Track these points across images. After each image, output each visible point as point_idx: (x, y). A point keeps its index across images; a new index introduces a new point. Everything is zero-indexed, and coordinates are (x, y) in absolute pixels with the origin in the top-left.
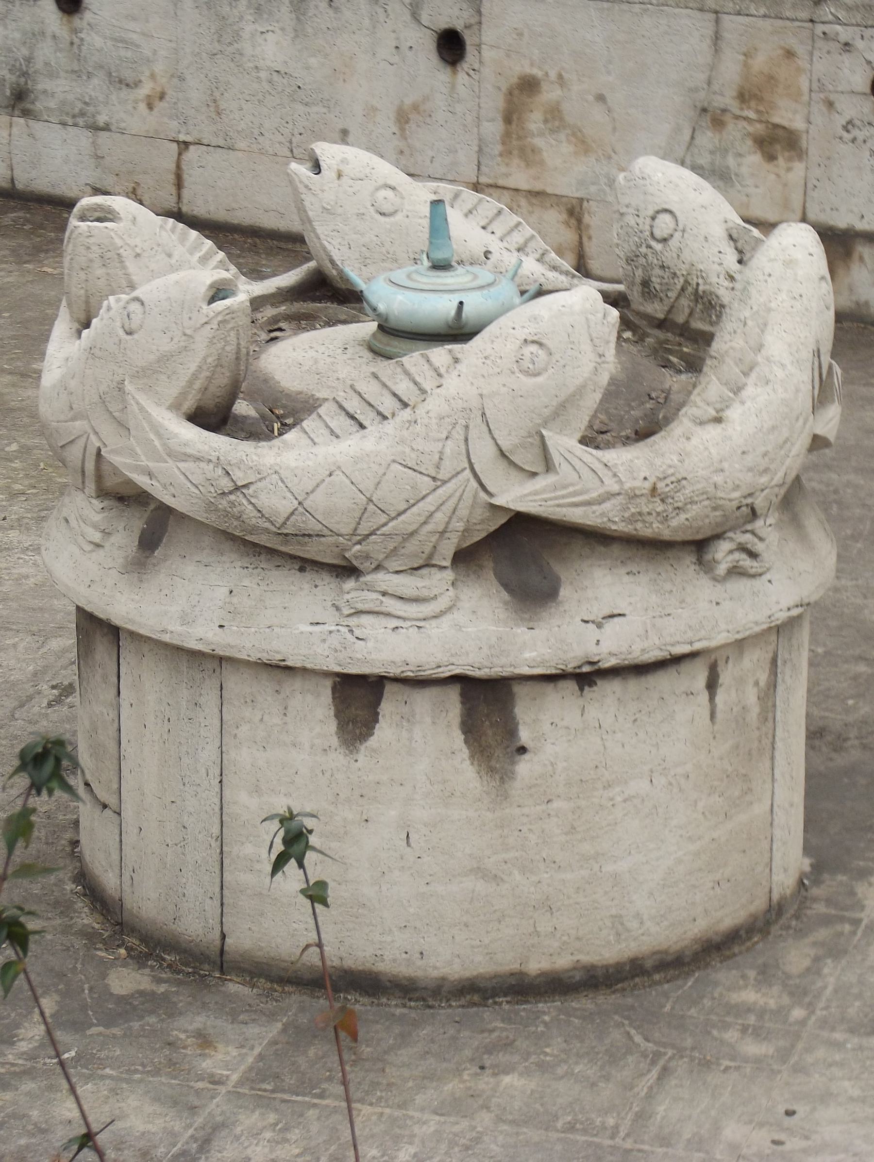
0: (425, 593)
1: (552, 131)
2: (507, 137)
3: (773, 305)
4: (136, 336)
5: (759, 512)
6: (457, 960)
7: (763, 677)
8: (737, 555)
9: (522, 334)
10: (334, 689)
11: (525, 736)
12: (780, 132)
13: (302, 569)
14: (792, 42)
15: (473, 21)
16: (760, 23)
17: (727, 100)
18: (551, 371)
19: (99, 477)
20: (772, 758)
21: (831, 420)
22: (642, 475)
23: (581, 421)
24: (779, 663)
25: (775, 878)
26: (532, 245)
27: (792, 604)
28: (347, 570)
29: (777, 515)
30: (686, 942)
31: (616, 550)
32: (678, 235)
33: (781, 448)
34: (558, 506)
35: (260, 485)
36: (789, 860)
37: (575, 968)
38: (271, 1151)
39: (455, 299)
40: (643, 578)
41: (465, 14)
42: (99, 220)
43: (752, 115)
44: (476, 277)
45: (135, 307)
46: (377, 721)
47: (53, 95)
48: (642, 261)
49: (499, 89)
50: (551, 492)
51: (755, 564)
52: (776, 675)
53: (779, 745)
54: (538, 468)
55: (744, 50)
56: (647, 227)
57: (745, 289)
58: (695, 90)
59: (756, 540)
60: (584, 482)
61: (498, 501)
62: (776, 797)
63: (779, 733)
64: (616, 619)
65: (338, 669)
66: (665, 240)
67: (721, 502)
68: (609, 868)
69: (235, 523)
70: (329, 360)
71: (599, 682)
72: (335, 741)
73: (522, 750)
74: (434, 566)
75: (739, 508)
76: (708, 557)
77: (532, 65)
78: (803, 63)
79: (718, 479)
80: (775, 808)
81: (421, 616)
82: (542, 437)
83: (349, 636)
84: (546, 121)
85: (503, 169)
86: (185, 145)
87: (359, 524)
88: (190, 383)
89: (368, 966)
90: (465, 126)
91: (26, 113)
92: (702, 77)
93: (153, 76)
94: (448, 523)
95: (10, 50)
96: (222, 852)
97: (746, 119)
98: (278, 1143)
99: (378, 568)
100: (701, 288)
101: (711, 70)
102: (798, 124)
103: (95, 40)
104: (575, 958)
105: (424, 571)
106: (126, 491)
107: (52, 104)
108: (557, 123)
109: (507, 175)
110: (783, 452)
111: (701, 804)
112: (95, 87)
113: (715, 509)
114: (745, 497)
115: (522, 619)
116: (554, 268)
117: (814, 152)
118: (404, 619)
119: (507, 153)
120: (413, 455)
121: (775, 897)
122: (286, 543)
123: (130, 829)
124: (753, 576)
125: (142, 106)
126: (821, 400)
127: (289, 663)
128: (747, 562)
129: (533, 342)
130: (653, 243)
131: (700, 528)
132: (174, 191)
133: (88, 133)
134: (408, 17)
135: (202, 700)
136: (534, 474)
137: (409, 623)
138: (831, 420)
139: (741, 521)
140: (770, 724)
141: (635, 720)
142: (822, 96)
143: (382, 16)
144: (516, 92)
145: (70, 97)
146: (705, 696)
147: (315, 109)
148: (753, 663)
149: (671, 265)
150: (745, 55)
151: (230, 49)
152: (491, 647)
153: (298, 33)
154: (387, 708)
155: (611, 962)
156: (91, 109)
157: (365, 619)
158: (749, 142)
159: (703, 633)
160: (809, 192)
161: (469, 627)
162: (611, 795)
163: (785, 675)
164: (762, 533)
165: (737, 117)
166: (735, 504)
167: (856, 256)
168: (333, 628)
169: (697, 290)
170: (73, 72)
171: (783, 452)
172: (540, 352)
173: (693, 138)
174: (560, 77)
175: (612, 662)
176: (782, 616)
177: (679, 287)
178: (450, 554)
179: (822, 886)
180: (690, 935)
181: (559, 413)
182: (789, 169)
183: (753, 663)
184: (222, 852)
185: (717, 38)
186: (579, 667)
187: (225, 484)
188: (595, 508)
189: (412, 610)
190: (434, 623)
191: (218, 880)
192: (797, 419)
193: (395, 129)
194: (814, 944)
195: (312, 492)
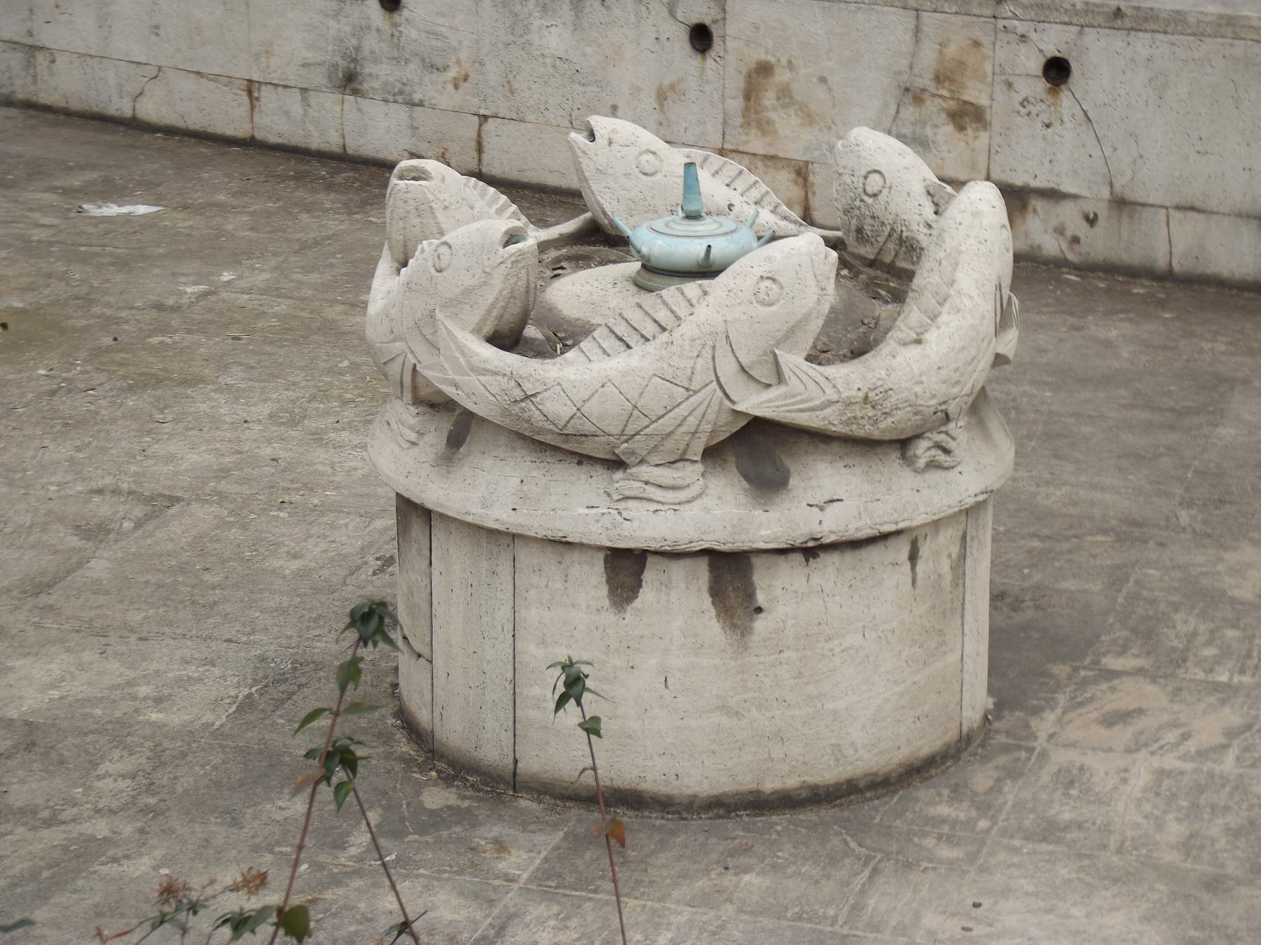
0: (680, 482)
1: (783, 107)
2: (747, 110)
4: (444, 273)
7: (955, 551)
9: (759, 272)
11: (761, 598)
12: (969, 108)
13: (580, 463)
14: (978, 34)
15: (719, 17)
16: (953, 18)
17: (926, 81)
18: (782, 302)
19: (415, 388)
20: (963, 617)
25: (964, 714)
26: (767, 199)
27: (978, 491)
28: (616, 464)
31: (835, 447)
32: (885, 191)
36: (976, 700)
38: (555, 936)
41: (713, 12)
43: (946, 93)
45: (444, 249)
46: (641, 586)
53: (968, 606)
58: (900, 73)
60: (810, 392)
61: (739, 408)
65: (609, 544)
72: (606, 603)
73: (759, 610)
76: (910, 453)
78: (987, 51)
81: (676, 501)
82: (775, 355)
83: (618, 517)
84: (778, 99)
85: (744, 138)
88: (489, 311)
89: (634, 786)
91: (355, 92)
93: (458, 62)
94: (698, 425)
97: (941, 96)
99: (642, 462)
102: (983, 101)
103: (411, 33)
105: (680, 465)
107: (377, 85)
108: (787, 100)
109: (747, 142)
111: (904, 654)
112: (412, 71)
113: (915, 414)
116: (785, 218)
117: (996, 124)
118: (663, 503)
119: (746, 125)
121: (965, 729)
122: (567, 441)
124: (947, 469)
125: (450, 87)
127: (569, 539)
128: (941, 457)
129: (768, 278)
130: (866, 198)
132: (475, 155)
134: (665, 14)
135: (499, 569)
136: (769, 386)
137: (667, 507)
140: (961, 589)
143: (645, 14)
144: (754, 75)
145: (391, 79)
146: (907, 566)
147: (590, 89)
148: (947, 540)
151: (521, 40)
153: (577, 27)
154: (648, 576)
156: (408, 89)
157: (631, 504)
158: (944, 116)
159: (906, 515)
160: (993, 156)
161: (717, 511)
163: (973, 549)
165: (934, 95)
166: (932, 410)
167: (1030, 208)
170: (394, 58)
173: (897, 112)
174: (790, 62)
180: (895, 760)
181: (789, 336)
182: (976, 138)
183: (947, 540)
187: (518, 394)
190: (687, 506)
193: (655, 105)
194: (997, 768)
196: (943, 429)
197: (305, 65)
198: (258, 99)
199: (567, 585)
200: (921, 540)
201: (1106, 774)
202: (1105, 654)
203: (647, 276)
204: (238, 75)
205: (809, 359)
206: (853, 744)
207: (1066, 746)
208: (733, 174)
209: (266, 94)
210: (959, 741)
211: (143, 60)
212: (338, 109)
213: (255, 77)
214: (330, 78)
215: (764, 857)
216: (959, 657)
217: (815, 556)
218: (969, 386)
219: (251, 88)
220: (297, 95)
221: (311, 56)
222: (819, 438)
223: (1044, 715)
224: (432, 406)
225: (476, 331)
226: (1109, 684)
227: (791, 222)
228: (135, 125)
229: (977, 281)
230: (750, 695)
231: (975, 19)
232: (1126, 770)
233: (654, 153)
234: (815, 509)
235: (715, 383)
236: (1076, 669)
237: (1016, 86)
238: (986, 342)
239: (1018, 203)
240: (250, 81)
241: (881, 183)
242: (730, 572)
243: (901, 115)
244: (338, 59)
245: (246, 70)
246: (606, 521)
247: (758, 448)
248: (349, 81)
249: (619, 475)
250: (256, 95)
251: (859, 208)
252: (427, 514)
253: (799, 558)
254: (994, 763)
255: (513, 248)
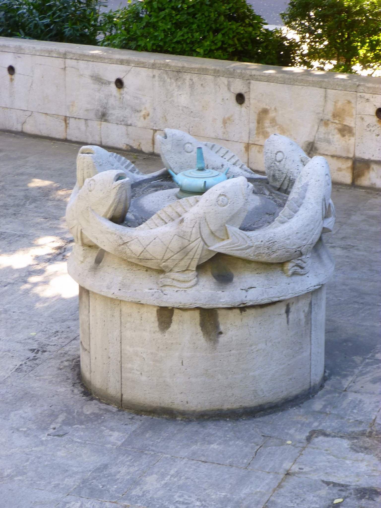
0: (187, 279)
1: (273, 126)
2: (258, 128)
3: (309, 183)
4: (92, 192)
5: (303, 253)
6: (199, 405)
7: (307, 309)
8: (296, 268)
9: (219, 192)
10: (157, 311)
11: (222, 328)
12: (347, 128)
13: (147, 271)
14: (349, 98)
15: (247, 91)
16: (339, 92)
17: (329, 116)
18: (229, 205)
19: (82, 239)
20: (310, 337)
21: (330, 222)
22: (261, 240)
23: (240, 221)
24: (313, 304)
25: (312, 378)
26: (238, 163)
27: (316, 284)
28: (161, 271)
29: (310, 254)
30: (279, 400)
31: (253, 265)
32: (284, 160)
33: (311, 231)
34: (232, 250)
35: (132, 242)
36: (317, 371)
37: (240, 408)
38: (128, 469)
39: (204, 180)
40: (263, 275)
41: (245, 89)
42: (88, 153)
43: (337, 122)
44: (212, 173)
45: (92, 182)
46: (171, 322)
47: (114, 115)
48: (272, 168)
49: (256, 112)
50: (229, 245)
51: (303, 271)
52: (311, 308)
53: (313, 332)
54: (226, 238)
55: (334, 101)
56: (274, 157)
57: (300, 178)
58: (318, 113)
59: (302, 263)
60: (234, 243)
61: (211, 248)
62: (312, 350)
63: (313, 328)
64: (253, 289)
65: (158, 305)
66: (280, 161)
67: (289, 250)
68: (251, 374)
69: (124, 255)
70: (163, 200)
71: (247, 310)
72: (157, 329)
73: (221, 333)
74: (190, 270)
75: (296, 252)
76: (285, 268)
77: (266, 105)
78: (353, 105)
79: (288, 242)
80: (312, 354)
81: (186, 287)
82: (226, 227)
83: (161, 293)
84: (271, 123)
85: (257, 139)
86: (155, 131)
87: (164, 255)
88: (109, 208)
89: (169, 406)
90: (245, 125)
91: (106, 121)
92: (322, 109)
93: (145, 108)
94: (194, 256)
95: (101, 101)
96: (121, 367)
97: (335, 123)
98: (131, 466)
99: (171, 271)
100: (291, 177)
101: (324, 107)
102: (352, 125)
103: (127, 97)
104: (241, 404)
105: (187, 272)
106: (91, 244)
107: (114, 117)
108: (274, 124)
109: (258, 141)
110: (311, 233)
111: (284, 352)
112: (127, 112)
113: (287, 252)
114: (298, 248)
115: (220, 288)
116: (246, 170)
117: (357, 134)
118: (180, 288)
119: (258, 134)
120: (182, 233)
121: (312, 384)
122: (141, 262)
123: (93, 358)
124: (302, 275)
125: (142, 118)
126: (326, 216)
127: (142, 302)
128: (299, 270)
129: (223, 195)
130: (276, 162)
131: (282, 258)
132: (152, 145)
133: (125, 127)
134: (226, 89)
135: (115, 314)
136: (223, 240)
137: (182, 289)
138: (330, 222)
139: (297, 256)
140: (309, 325)
141: (260, 324)
142: (360, 116)
143: (218, 89)
144: (261, 114)
145: (119, 115)
146: (285, 316)
147: (196, 119)
148: (303, 305)
149: (282, 170)
150: (335, 102)
151: (170, 100)
152: (209, 298)
153: (191, 95)
154: (174, 318)
155: (252, 406)
156: (126, 119)
157: (167, 288)
158: (336, 131)
159: (283, 294)
160: (356, 147)
161: (206, 292)
162: (252, 348)
163: (315, 309)
164: (305, 260)
165: (333, 122)
166: (294, 250)
167: (371, 169)
168: (157, 291)
169: (290, 178)
170: (120, 107)
171: (311, 233)
172: (225, 198)
173: (318, 129)
174: (275, 109)
175: (251, 303)
176: (313, 288)
177: (284, 177)
178: (195, 266)
179: (331, 381)
180: (281, 397)
181: (231, 219)
182: (349, 140)
183: (303, 305)
184: (121, 367)
185: (326, 97)
186: (239, 305)
187: (120, 242)
188: (244, 251)
189: (183, 285)
190: (190, 289)
191: (120, 376)
192: (317, 222)
193: (222, 125)
194: (325, 400)
195: (149, 244)
196: (300, 258)
197: (87, 110)
198: (68, 123)
199: (142, 321)
200: (291, 305)
201: (370, 403)
202: (377, 353)
203: (181, 193)
204: (61, 114)
205: (240, 228)
206: (262, 390)
207: (356, 392)
208: (225, 152)
209: (72, 122)
210: (310, 389)
211: (26, 109)
212: (99, 127)
213: (68, 115)
214: (96, 115)
215: (221, 437)
216: (309, 353)
217: (245, 311)
218: (311, 240)
219: (66, 119)
220: (83, 121)
221: (89, 107)
222: (246, 261)
223: (348, 378)
224: (90, 246)
225: (105, 216)
226: (377, 366)
227: (248, 172)
228: (22, 134)
229: (314, 197)
230: (218, 369)
231: (348, 92)
232: (378, 402)
233: (191, 144)
234: (244, 291)
235: (200, 238)
236: (365, 359)
237: (365, 119)
238: (318, 222)
239: (366, 166)
240: (66, 117)
241: (282, 156)
242: (209, 318)
243: (319, 130)
244: (99, 108)
245: (64, 112)
246: (156, 295)
247: (219, 267)
248: (103, 116)
249: (162, 276)
250: (68, 122)
251: (274, 166)
252: (88, 292)
253: (238, 311)
254: (323, 399)
255: (120, 182)
